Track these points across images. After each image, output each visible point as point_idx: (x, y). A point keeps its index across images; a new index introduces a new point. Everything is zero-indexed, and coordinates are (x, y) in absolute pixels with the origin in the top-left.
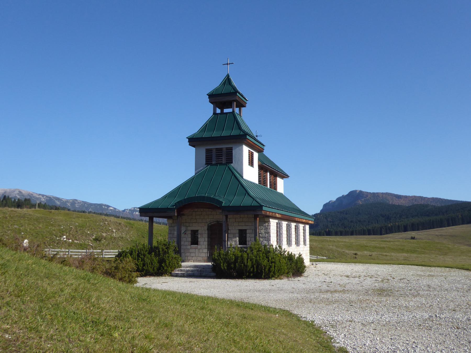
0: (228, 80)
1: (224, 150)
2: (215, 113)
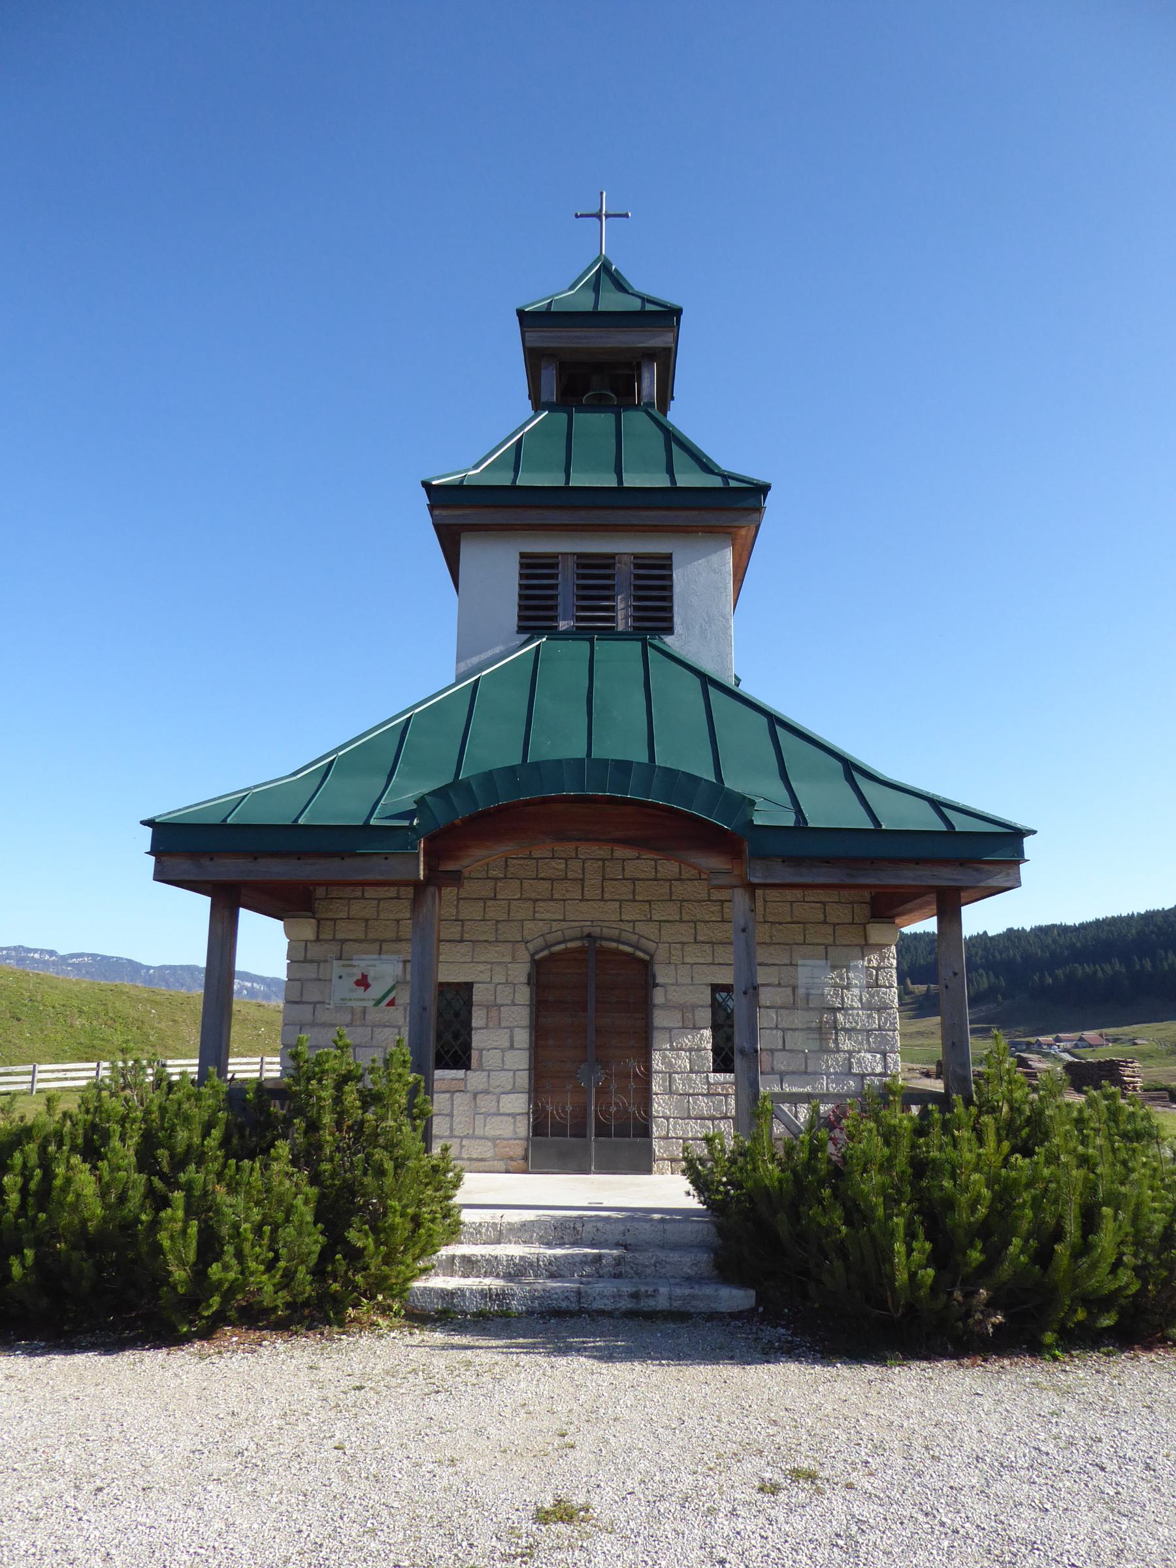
1: (624, 572)
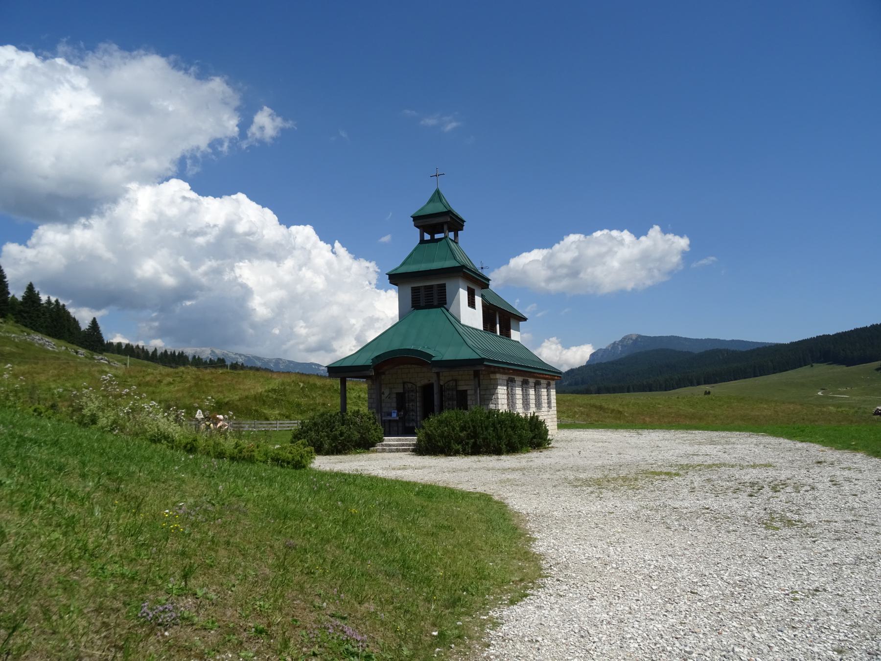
0: (438, 196)
2: (422, 241)
